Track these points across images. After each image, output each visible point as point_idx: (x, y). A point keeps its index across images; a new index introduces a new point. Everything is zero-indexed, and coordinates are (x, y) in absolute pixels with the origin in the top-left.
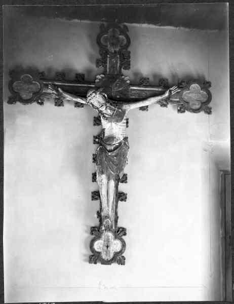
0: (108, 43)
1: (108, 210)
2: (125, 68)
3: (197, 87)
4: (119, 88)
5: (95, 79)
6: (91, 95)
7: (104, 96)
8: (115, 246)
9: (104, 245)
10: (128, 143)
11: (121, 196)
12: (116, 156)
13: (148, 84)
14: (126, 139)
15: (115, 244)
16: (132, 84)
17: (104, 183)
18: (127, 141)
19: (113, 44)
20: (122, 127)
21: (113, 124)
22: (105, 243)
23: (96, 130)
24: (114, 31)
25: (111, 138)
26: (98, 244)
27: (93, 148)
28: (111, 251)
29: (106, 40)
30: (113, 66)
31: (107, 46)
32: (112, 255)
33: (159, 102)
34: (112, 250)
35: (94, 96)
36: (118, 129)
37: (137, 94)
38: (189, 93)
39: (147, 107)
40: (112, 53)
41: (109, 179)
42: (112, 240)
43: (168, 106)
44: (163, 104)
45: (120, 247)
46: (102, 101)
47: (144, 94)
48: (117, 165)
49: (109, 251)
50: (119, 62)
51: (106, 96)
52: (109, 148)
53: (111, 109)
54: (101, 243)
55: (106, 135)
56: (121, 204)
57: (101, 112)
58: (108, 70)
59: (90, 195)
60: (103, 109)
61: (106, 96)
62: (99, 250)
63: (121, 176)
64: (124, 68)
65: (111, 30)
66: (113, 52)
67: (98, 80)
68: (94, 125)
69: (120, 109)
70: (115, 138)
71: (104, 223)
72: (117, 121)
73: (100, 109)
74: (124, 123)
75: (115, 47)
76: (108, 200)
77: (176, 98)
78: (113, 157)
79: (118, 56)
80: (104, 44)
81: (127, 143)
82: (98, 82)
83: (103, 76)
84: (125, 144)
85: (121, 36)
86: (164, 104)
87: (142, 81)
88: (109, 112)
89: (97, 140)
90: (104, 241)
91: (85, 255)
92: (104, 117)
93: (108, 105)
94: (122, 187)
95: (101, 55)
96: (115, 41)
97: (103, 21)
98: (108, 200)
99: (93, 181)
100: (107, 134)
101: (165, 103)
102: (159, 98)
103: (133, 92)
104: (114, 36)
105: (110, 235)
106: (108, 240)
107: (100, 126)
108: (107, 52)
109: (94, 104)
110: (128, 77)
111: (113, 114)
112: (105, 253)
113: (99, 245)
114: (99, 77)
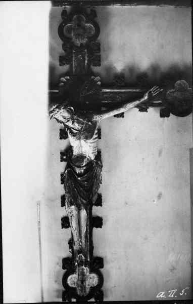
0: (72, 35)
1: (81, 242)
2: (95, 65)
3: (184, 83)
4: (88, 91)
5: (59, 83)
6: (54, 110)
7: (70, 109)
8: (91, 280)
9: (78, 280)
10: (101, 163)
11: (96, 222)
12: (86, 181)
13: (123, 84)
14: (98, 156)
15: (91, 278)
16: (105, 85)
17: (74, 215)
18: (101, 161)
19: (78, 36)
20: (93, 144)
21: (82, 141)
22: (80, 277)
23: (63, 145)
24: (79, 19)
25: (81, 157)
26: (71, 278)
27: (61, 167)
28: (87, 286)
29: (70, 30)
30: (80, 63)
31: (71, 39)
32: (88, 290)
33: (137, 106)
34: (88, 285)
35: (58, 112)
36: (89, 148)
37: (110, 97)
38: (173, 92)
39: (123, 113)
40: (77, 47)
41: (79, 209)
42: (88, 274)
43: (148, 110)
44: (143, 108)
45: (97, 281)
46: (66, 115)
47: (119, 99)
48: (87, 191)
49: (85, 286)
50: (86, 58)
51: (72, 108)
52: (78, 171)
53: (79, 122)
54: (75, 277)
55: (74, 153)
56: (96, 230)
57: (67, 126)
58: (74, 69)
59: (60, 222)
60: (70, 124)
61: (72, 108)
62: (73, 286)
63: (95, 198)
64: (93, 65)
65: (75, 16)
66: (79, 45)
67: (62, 84)
68: (61, 138)
69: (89, 121)
70: (86, 157)
71: (77, 259)
72: (87, 138)
73: (67, 124)
74: (96, 138)
75: (82, 39)
76: (80, 232)
77: (159, 100)
78: (84, 181)
79: (86, 50)
80: (68, 36)
81: (99, 162)
82: (62, 86)
83: (68, 77)
84: (97, 163)
85: (88, 25)
86: (144, 108)
87: (119, 80)
88: (77, 126)
89: (65, 157)
90: (79, 275)
91: (104, 51)
92: (71, 132)
93: (75, 117)
94: (96, 211)
95: (65, 50)
96: (81, 31)
97: (65, 5)
98: (80, 232)
99: (62, 206)
100: (76, 152)
101: (144, 107)
102: (137, 102)
103: (105, 96)
104: (79, 25)
105: (86, 269)
106: (82, 274)
107: (67, 140)
108: (73, 46)
109: (58, 119)
110: (99, 77)
111: (81, 129)
112: (80, 288)
113: (73, 279)
114: (63, 79)
